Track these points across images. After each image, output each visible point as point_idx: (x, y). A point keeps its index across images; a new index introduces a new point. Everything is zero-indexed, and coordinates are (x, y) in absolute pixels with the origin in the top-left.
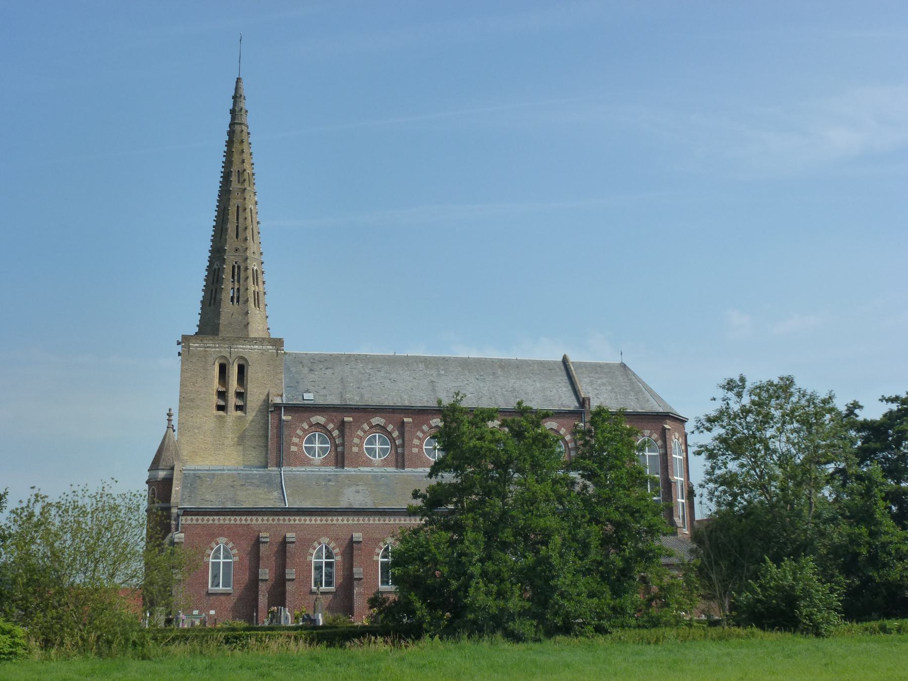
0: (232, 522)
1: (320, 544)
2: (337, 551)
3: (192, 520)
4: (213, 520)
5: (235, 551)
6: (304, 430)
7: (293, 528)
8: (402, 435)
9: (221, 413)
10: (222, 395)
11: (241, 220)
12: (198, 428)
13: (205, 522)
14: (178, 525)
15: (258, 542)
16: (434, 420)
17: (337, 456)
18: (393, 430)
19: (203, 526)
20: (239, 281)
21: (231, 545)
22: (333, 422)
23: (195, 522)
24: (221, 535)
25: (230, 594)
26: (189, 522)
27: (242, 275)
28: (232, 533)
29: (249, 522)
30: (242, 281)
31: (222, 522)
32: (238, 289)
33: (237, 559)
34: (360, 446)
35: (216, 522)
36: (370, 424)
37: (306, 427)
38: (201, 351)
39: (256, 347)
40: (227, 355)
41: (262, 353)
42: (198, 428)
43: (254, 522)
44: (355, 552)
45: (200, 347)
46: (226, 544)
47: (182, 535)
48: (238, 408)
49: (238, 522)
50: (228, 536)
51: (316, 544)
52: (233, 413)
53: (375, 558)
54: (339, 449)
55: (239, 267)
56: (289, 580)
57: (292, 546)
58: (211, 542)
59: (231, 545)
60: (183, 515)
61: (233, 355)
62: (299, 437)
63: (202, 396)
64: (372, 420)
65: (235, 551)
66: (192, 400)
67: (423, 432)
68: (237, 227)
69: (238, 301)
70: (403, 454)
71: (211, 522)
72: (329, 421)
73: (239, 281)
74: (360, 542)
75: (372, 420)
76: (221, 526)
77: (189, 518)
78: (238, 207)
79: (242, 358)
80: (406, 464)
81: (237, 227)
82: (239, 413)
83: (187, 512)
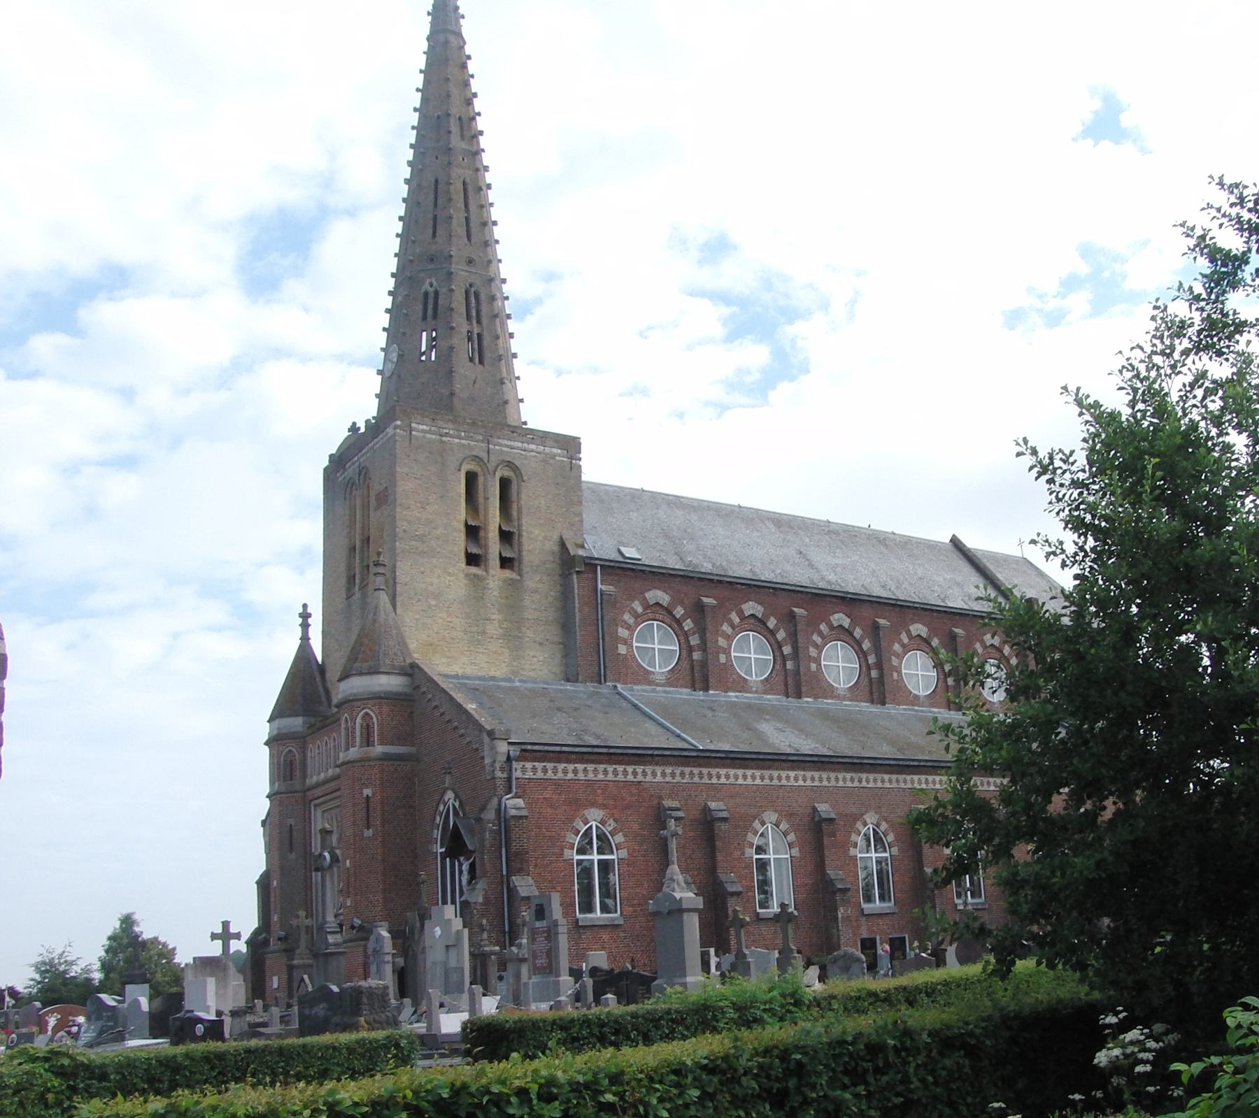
0: (610, 777)
1: (763, 823)
2: (891, 838)
3: (534, 769)
4: (575, 772)
5: (619, 838)
6: (636, 616)
7: (715, 790)
8: (793, 637)
9: (473, 570)
10: (473, 532)
11: (472, 208)
12: (437, 596)
13: (560, 775)
14: (509, 779)
15: (660, 817)
16: (836, 616)
17: (692, 668)
18: (777, 628)
19: (557, 784)
20: (479, 322)
21: (611, 825)
22: (682, 604)
23: (540, 775)
24: (593, 804)
25: (617, 926)
26: (529, 774)
27: (485, 309)
28: (615, 800)
29: (640, 778)
30: (485, 321)
31: (591, 776)
32: (479, 336)
33: (623, 853)
34: (728, 653)
35: (581, 776)
36: (740, 613)
37: (640, 610)
38: (430, 442)
39: (533, 447)
40: (484, 455)
41: (544, 461)
42: (437, 596)
43: (649, 778)
44: (826, 841)
45: (429, 432)
46: (603, 822)
47: (520, 802)
48: (506, 563)
49: (621, 777)
50: (604, 807)
51: (756, 824)
52: (496, 576)
53: (567, 852)
54: (696, 656)
55: (477, 295)
56: (733, 894)
57: (724, 826)
58: (571, 820)
59: (611, 825)
60: (518, 759)
61: (492, 458)
62: (629, 627)
63: (439, 531)
64: (744, 607)
65: (619, 838)
66: (421, 538)
67: (820, 634)
68: (467, 219)
69: (481, 362)
70: (797, 672)
71: (570, 776)
72: (677, 601)
73: (479, 322)
74: (832, 820)
75: (744, 607)
76: (589, 784)
77: (529, 765)
78: (464, 183)
79: (510, 465)
80: (804, 689)
81: (467, 219)
82: (508, 574)
83: (530, 753)
